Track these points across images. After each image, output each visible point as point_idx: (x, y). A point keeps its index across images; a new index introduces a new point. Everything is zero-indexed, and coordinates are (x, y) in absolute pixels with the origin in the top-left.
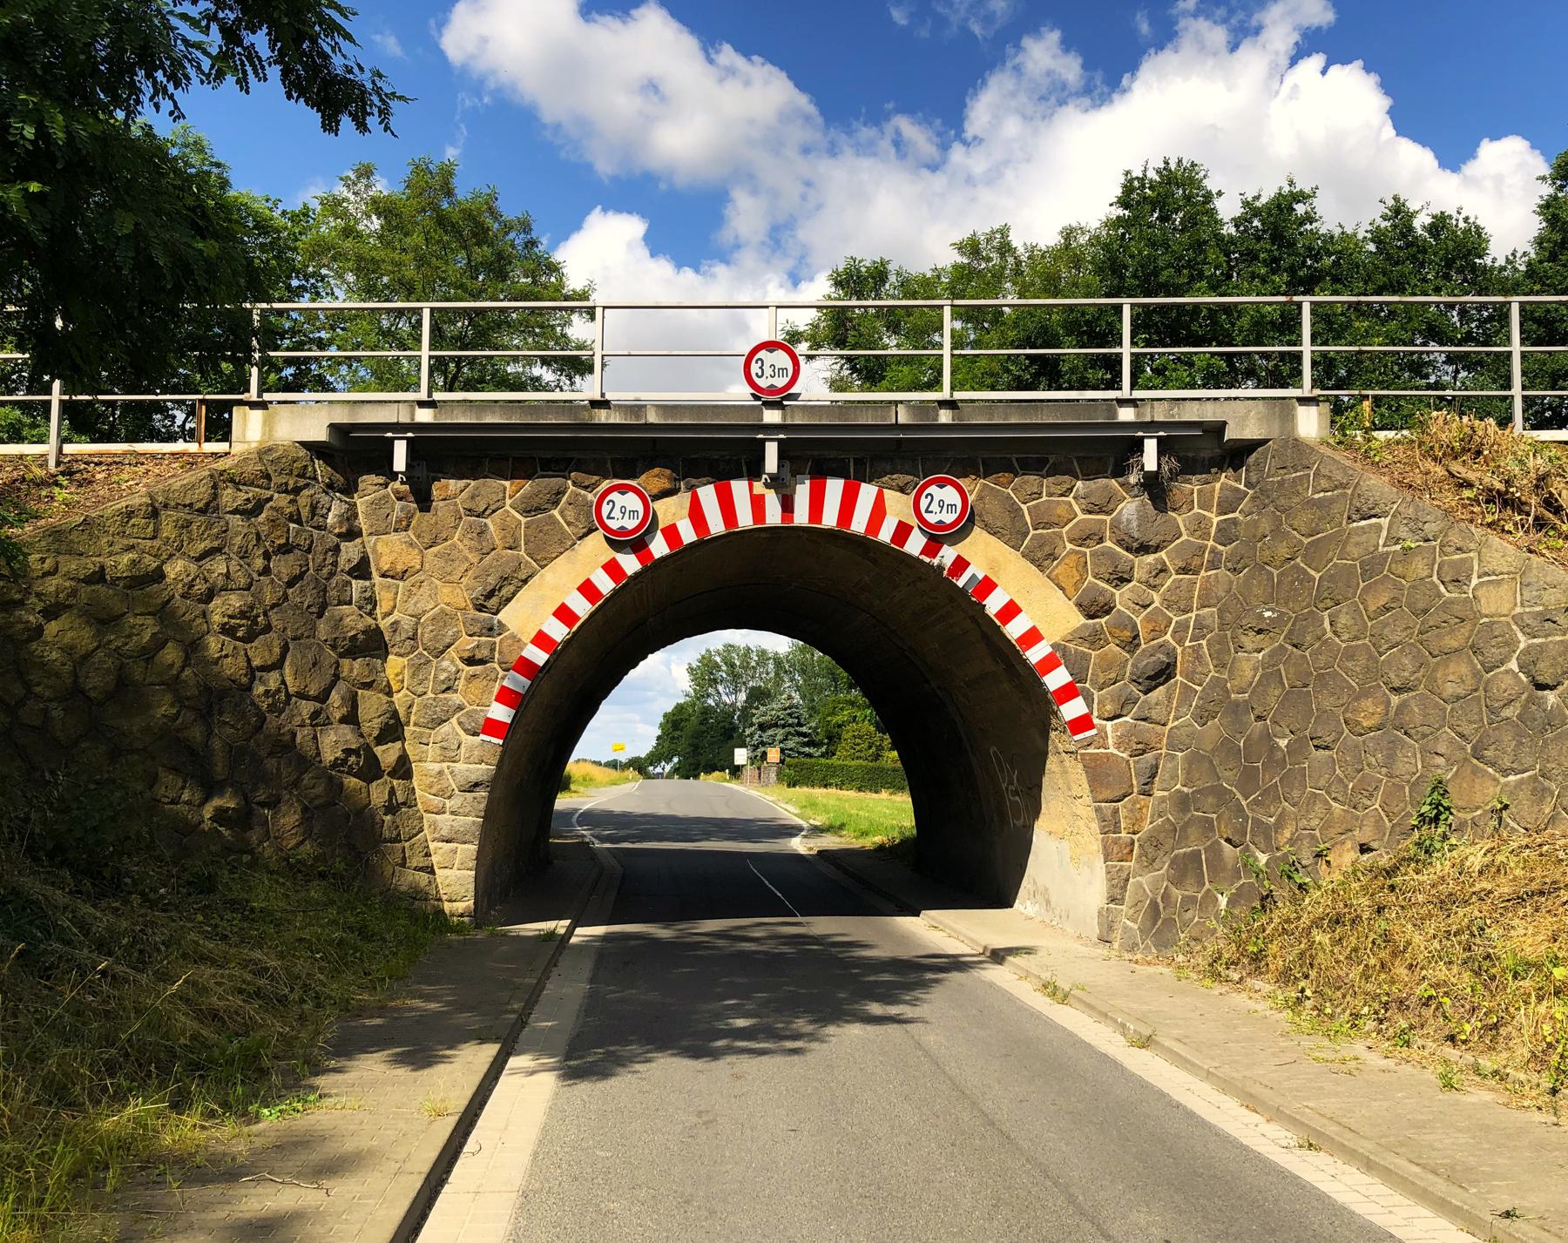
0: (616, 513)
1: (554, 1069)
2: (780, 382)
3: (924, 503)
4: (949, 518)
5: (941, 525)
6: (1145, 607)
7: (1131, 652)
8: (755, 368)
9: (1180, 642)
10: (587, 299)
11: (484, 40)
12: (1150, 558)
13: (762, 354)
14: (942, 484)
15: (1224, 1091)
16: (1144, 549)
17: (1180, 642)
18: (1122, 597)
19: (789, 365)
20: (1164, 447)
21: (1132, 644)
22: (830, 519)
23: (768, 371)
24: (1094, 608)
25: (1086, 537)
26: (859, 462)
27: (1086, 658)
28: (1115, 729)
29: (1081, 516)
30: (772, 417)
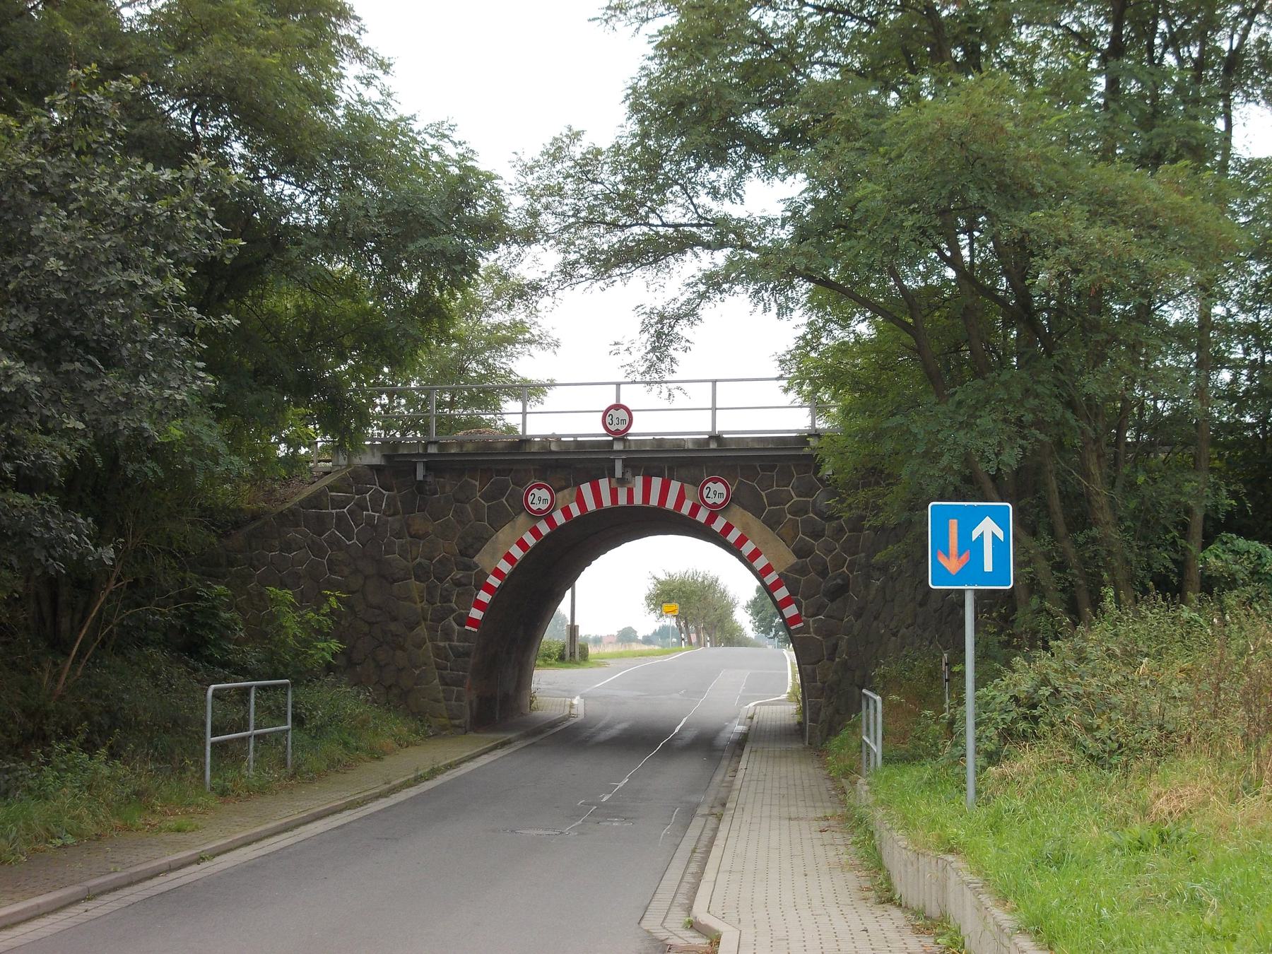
0: (536, 501)
1: (602, 729)
2: (622, 427)
3: (705, 492)
4: (719, 501)
5: (715, 505)
6: (831, 552)
7: (824, 578)
8: (608, 420)
9: (851, 572)
10: (106, 367)
11: (783, 311)
12: (834, 524)
13: (612, 412)
14: (715, 481)
15: (706, 926)
16: (831, 518)
17: (851, 572)
18: (818, 546)
19: (627, 418)
20: (428, 467)
21: (823, 573)
22: (654, 501)
23: (615, 421)
24: (800, 552)
25: (799, 510)
26: (671, 469)
27: (798, 581)
28: (814, 622)
29: (796, 499)
30: (618, 446)
